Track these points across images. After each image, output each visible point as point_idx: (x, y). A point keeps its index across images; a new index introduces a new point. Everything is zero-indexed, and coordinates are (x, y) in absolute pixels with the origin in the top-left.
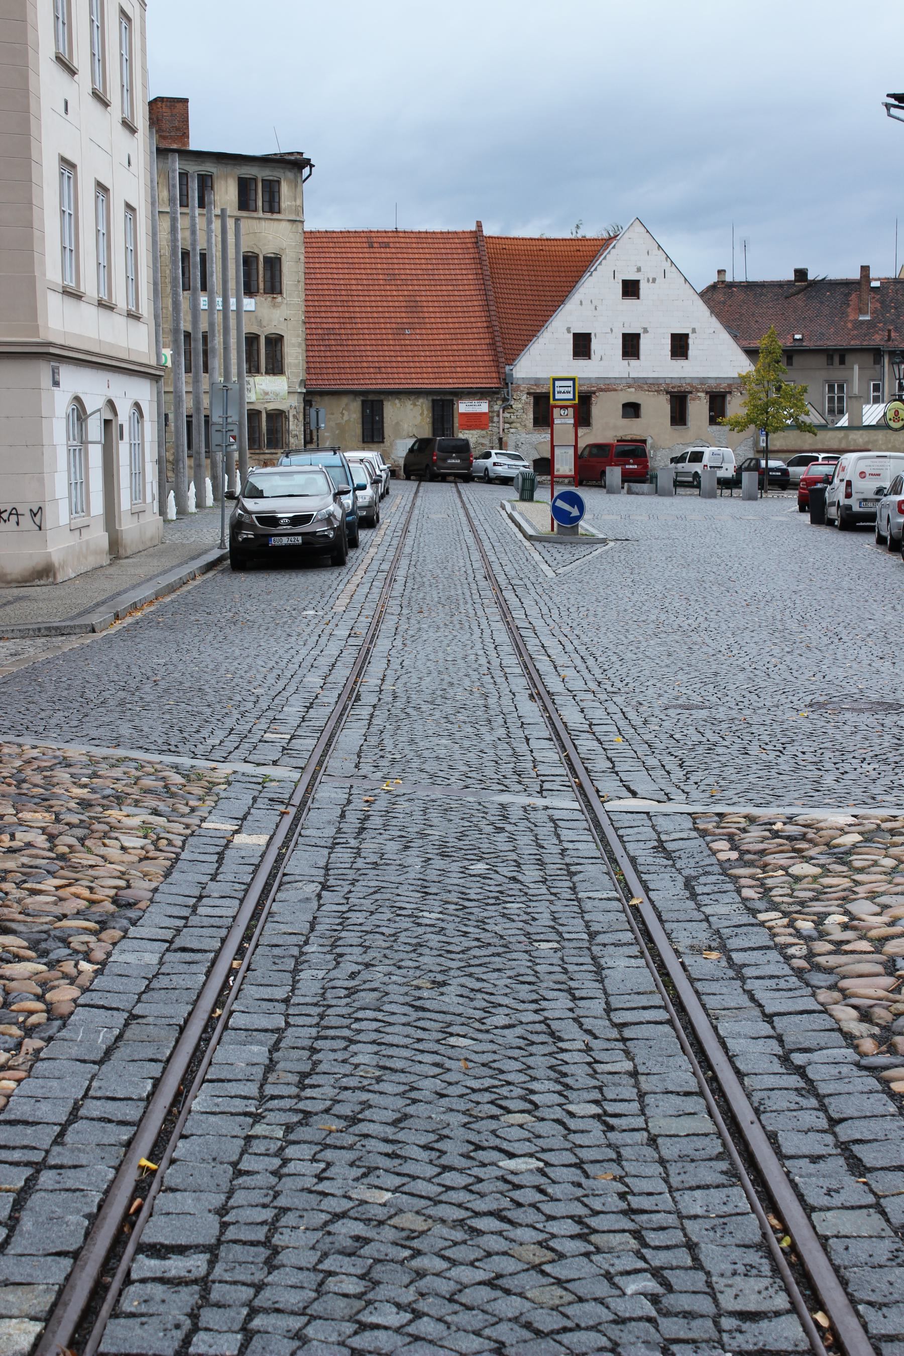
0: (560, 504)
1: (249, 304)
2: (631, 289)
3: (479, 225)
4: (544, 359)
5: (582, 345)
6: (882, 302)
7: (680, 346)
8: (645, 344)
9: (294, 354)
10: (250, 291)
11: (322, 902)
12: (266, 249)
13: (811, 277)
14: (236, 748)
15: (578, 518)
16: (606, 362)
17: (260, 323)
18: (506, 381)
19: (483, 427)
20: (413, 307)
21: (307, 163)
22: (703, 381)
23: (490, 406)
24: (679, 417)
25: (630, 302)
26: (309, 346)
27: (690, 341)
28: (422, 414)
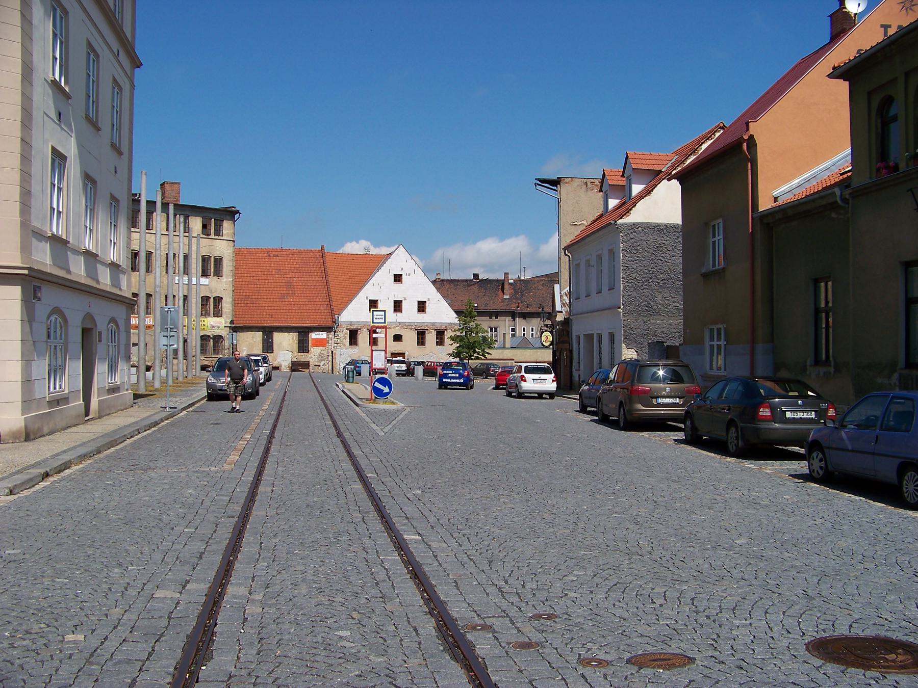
1: (204, 281)
2: (398, 278)
3: (323, 247)
4: (355, 313)
5: (373, 304)
7: (421, 307)
9: (227, 306)
10: (205, 274)
12: (216, 253)
14: (145, 584)
15: (388, 394)
17: (211, 291)
20: (289, 285)
21: (238, 212)
22: (433, 324)
24: (421, 340)
25: (398, 285)
26: (235, 304)
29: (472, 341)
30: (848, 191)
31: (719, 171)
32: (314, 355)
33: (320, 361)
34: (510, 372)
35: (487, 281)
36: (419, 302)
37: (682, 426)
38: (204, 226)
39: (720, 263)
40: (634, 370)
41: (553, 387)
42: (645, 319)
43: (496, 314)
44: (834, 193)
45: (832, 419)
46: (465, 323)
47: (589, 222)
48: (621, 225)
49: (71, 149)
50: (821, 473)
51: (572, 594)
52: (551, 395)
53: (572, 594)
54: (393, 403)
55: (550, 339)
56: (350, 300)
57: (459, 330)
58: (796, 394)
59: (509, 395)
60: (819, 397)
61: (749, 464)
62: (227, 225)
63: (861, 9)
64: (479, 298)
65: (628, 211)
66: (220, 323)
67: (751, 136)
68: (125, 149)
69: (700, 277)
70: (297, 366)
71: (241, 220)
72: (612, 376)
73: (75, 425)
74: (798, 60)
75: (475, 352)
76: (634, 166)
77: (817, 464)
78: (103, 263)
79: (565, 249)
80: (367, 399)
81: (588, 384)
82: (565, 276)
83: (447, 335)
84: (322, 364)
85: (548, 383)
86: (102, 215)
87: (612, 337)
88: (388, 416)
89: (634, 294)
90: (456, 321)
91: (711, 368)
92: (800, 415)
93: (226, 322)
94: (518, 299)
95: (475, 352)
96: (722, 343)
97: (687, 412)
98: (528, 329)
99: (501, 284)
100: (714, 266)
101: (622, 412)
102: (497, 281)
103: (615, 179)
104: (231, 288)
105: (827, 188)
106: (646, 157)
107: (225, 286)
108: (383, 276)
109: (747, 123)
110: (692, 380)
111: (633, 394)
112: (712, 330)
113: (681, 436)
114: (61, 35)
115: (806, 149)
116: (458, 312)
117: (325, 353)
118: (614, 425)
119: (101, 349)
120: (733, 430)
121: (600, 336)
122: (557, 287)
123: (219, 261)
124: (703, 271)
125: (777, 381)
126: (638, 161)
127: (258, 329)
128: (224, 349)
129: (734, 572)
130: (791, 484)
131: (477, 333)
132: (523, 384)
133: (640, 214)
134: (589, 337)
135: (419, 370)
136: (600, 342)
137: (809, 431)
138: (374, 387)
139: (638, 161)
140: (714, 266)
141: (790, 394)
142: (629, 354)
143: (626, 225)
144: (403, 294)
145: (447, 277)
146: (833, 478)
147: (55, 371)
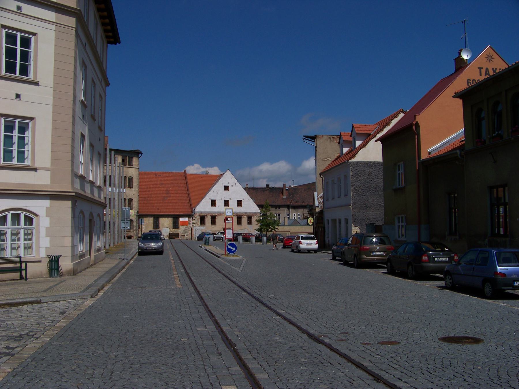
0: (229, 247)
2: (227, 188)
4: (203, 207)
5: (213, 203)
7: (240, 203)
8: (230, 203)
9: (135, 204)
15: (234, 251)
16: (220, 207)
18: (193, 212)
19: (187, 225)
21: (141, 153)
22: (246, 213)
24: (239, 222)
27: (230, 202)
29: (268, 222)
30: (463, 152)
31: (402, 140)
32: (181, 229)
33: (185, 233)
34: (293, 239)
35: (274, 189)
36: (238, 201)
37: (385, 266)
38: (123, 161)
39: (402, 185)
40: (360, 239)
41: (316, 247)
42: (364, 211)
43: (278, 207)
44: (457, 153)
45: (455, 261)
46: (264, 212)
47: (333, 160)
48: (351, 163)
49: (86, 133)
50: (450, 285)
51: (352, 327)
52: (315, 251)
53: (352, 327)
54: (237, 256)
55: (313, 221)
56: (201, 200)
57: (261, 216)
58: (440, 249)
59: (293, 251)
60: (450, 251)
61: (418, 283)
62: (135, 160)
63: (468, 58)
64: (269, 198)
65: (354, 156)
67: (417, 122)
68: (103, 128)
69: (393, 191)
70: (172, 236)
71: (143, 157)
72: (350, 242)
73: (88, 268)
74: (439, 80)
75: (270, 228)
76: (357, 132)
77: (448, 281)
78: (95, 187)
79: (320, 174)
80: (223, 254)
81: (336, 245)
82: (320, 186)
83: (254, 219)
84: (186, 235)
85: (313, 245)
86: (95, 162)
87: (346, 221)
88: (237, 263)
89: (358, 198)
90: (259, 211)
91: (399, 237)
92: (441, 259)
93: (134, 212)
94: (293, 197)
95: (270, 228)
96: (404, 224)
97: (388, 259)
99: (281, 190)
100: (399, 185)
101: (356, 259)
102: (279, 188)
103: (346, 137)
104: (137, 194)
105: (453, 150)
106: (363, 127)
107: (134, 193)
108: (219, 187)
109: (415, 116)
110: (390, 243)
111: (361, 250)
112: (399, 218)
113: (385, 270)
114: (85, 79)
115: (443, 131)
116: (260, 206)
118: (352, 266)
119: (95, 229)
120: (410, 267)
121: (340, 220)
122: (316, 194)
123: (131, 179)
124: (394, 188)
125: (432, 244)
126: (359, 129)
129: (413, 320)
130: (437, 290)
131: (271, 218)
132: (301, 246)
133: (360, 157)
134: (334, 221)
135: (240, 238)
136: (340, 223)
137: (445, 267)
138: (228, 248)
139: (359, 129)
140: (399, 185)
141: (437, 250)
142: (355, 230)
143: (353, 162)
144: (228, 197)
145: (252, 186)
146: (454, 287)
147: (81, 240)
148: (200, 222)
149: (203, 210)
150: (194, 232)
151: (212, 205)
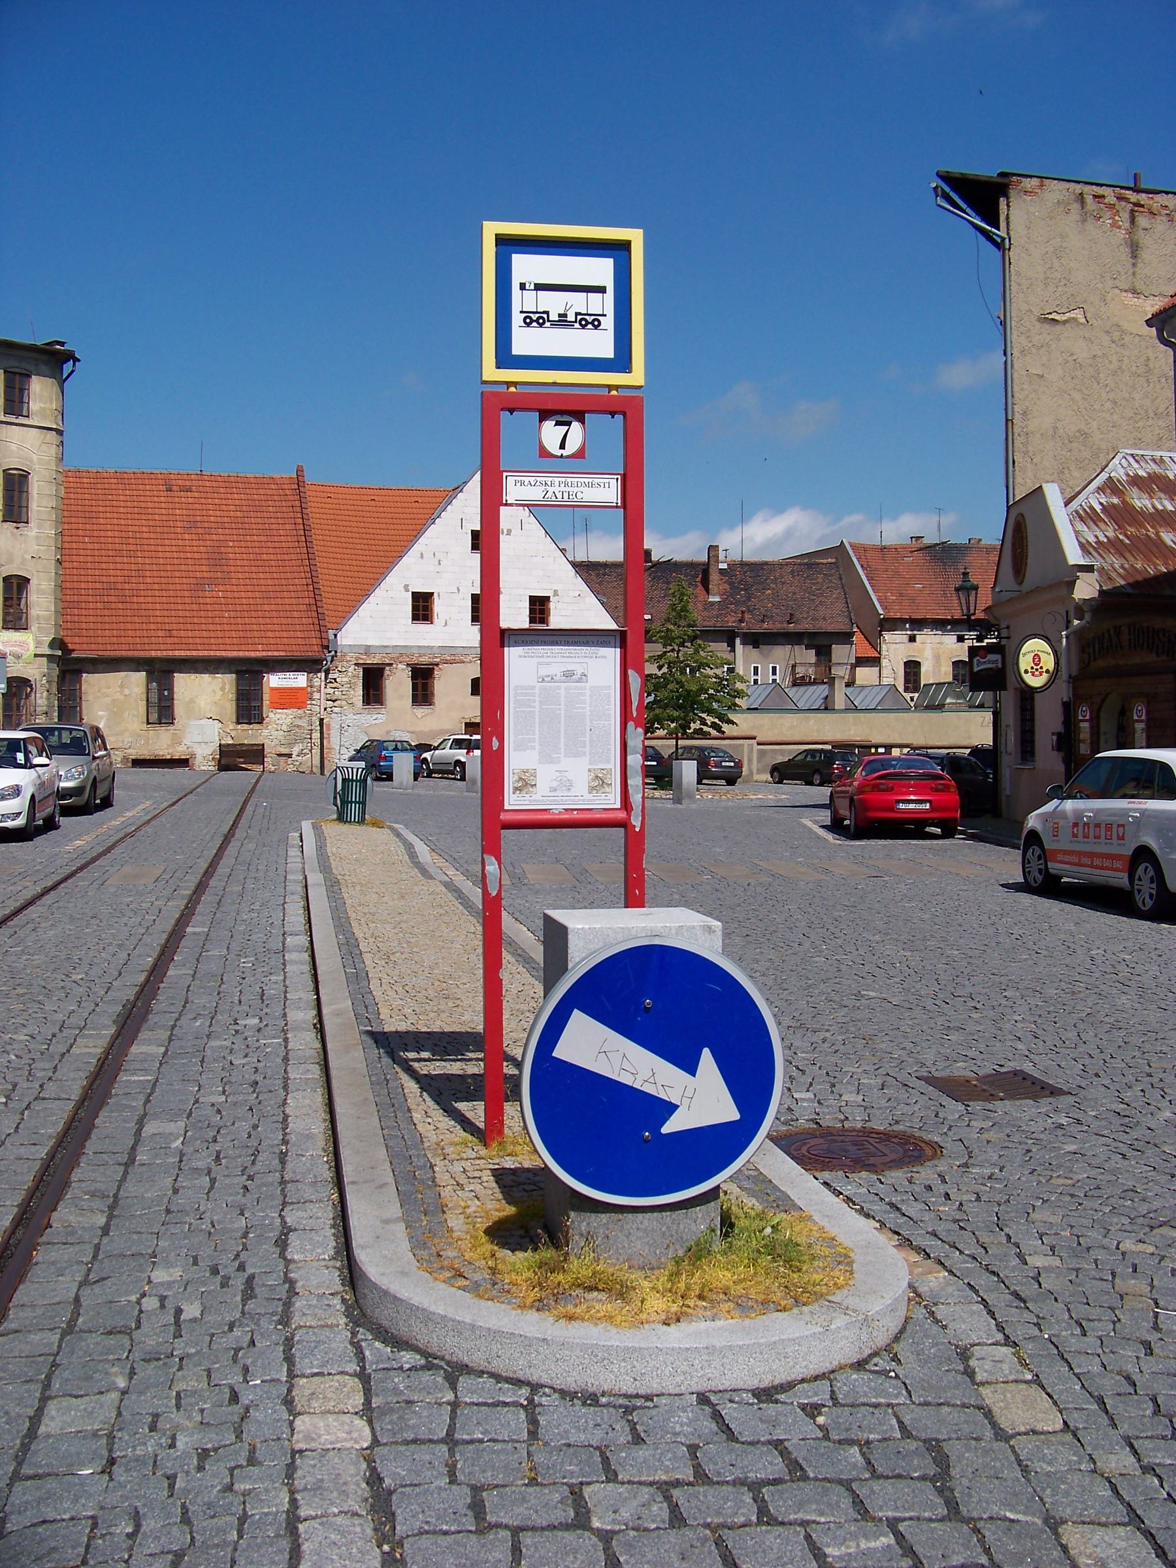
0: (590, 1045)
3: (300, 470)
4: (376, 624)
5: (422, 607)
6: (731, 584)
9: (41, 601)
11: (48, 1393)
13: (655, 557)
15: (717, 1146)
19: (301, 705)
21: (70, 356)
23: (309, 680)
27: (552, 605)
28: (222, 689)
32: (276, 728)
55: (1048, 662)
66: (21, 644)
70: (232, 758)
71: (80, 377)
84: (296, 750)
93: (38, 643)
98: (765, 668)
102: (691, 565)
104: (50, 555)
107: (34, 548)
117: (303, 723)
127: (135, 664)
128: (34, 714)
148: (360, 691)
149: (373, 641)
150: (334, 740)
151: (416, 617)
